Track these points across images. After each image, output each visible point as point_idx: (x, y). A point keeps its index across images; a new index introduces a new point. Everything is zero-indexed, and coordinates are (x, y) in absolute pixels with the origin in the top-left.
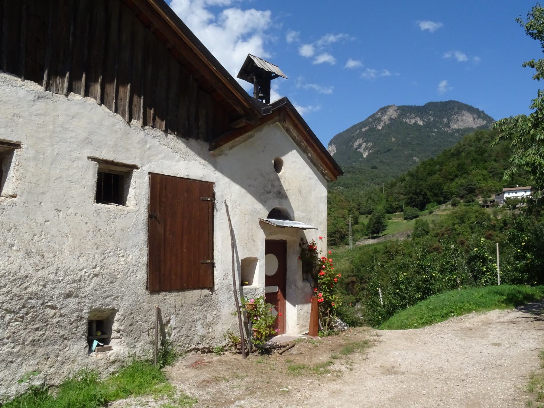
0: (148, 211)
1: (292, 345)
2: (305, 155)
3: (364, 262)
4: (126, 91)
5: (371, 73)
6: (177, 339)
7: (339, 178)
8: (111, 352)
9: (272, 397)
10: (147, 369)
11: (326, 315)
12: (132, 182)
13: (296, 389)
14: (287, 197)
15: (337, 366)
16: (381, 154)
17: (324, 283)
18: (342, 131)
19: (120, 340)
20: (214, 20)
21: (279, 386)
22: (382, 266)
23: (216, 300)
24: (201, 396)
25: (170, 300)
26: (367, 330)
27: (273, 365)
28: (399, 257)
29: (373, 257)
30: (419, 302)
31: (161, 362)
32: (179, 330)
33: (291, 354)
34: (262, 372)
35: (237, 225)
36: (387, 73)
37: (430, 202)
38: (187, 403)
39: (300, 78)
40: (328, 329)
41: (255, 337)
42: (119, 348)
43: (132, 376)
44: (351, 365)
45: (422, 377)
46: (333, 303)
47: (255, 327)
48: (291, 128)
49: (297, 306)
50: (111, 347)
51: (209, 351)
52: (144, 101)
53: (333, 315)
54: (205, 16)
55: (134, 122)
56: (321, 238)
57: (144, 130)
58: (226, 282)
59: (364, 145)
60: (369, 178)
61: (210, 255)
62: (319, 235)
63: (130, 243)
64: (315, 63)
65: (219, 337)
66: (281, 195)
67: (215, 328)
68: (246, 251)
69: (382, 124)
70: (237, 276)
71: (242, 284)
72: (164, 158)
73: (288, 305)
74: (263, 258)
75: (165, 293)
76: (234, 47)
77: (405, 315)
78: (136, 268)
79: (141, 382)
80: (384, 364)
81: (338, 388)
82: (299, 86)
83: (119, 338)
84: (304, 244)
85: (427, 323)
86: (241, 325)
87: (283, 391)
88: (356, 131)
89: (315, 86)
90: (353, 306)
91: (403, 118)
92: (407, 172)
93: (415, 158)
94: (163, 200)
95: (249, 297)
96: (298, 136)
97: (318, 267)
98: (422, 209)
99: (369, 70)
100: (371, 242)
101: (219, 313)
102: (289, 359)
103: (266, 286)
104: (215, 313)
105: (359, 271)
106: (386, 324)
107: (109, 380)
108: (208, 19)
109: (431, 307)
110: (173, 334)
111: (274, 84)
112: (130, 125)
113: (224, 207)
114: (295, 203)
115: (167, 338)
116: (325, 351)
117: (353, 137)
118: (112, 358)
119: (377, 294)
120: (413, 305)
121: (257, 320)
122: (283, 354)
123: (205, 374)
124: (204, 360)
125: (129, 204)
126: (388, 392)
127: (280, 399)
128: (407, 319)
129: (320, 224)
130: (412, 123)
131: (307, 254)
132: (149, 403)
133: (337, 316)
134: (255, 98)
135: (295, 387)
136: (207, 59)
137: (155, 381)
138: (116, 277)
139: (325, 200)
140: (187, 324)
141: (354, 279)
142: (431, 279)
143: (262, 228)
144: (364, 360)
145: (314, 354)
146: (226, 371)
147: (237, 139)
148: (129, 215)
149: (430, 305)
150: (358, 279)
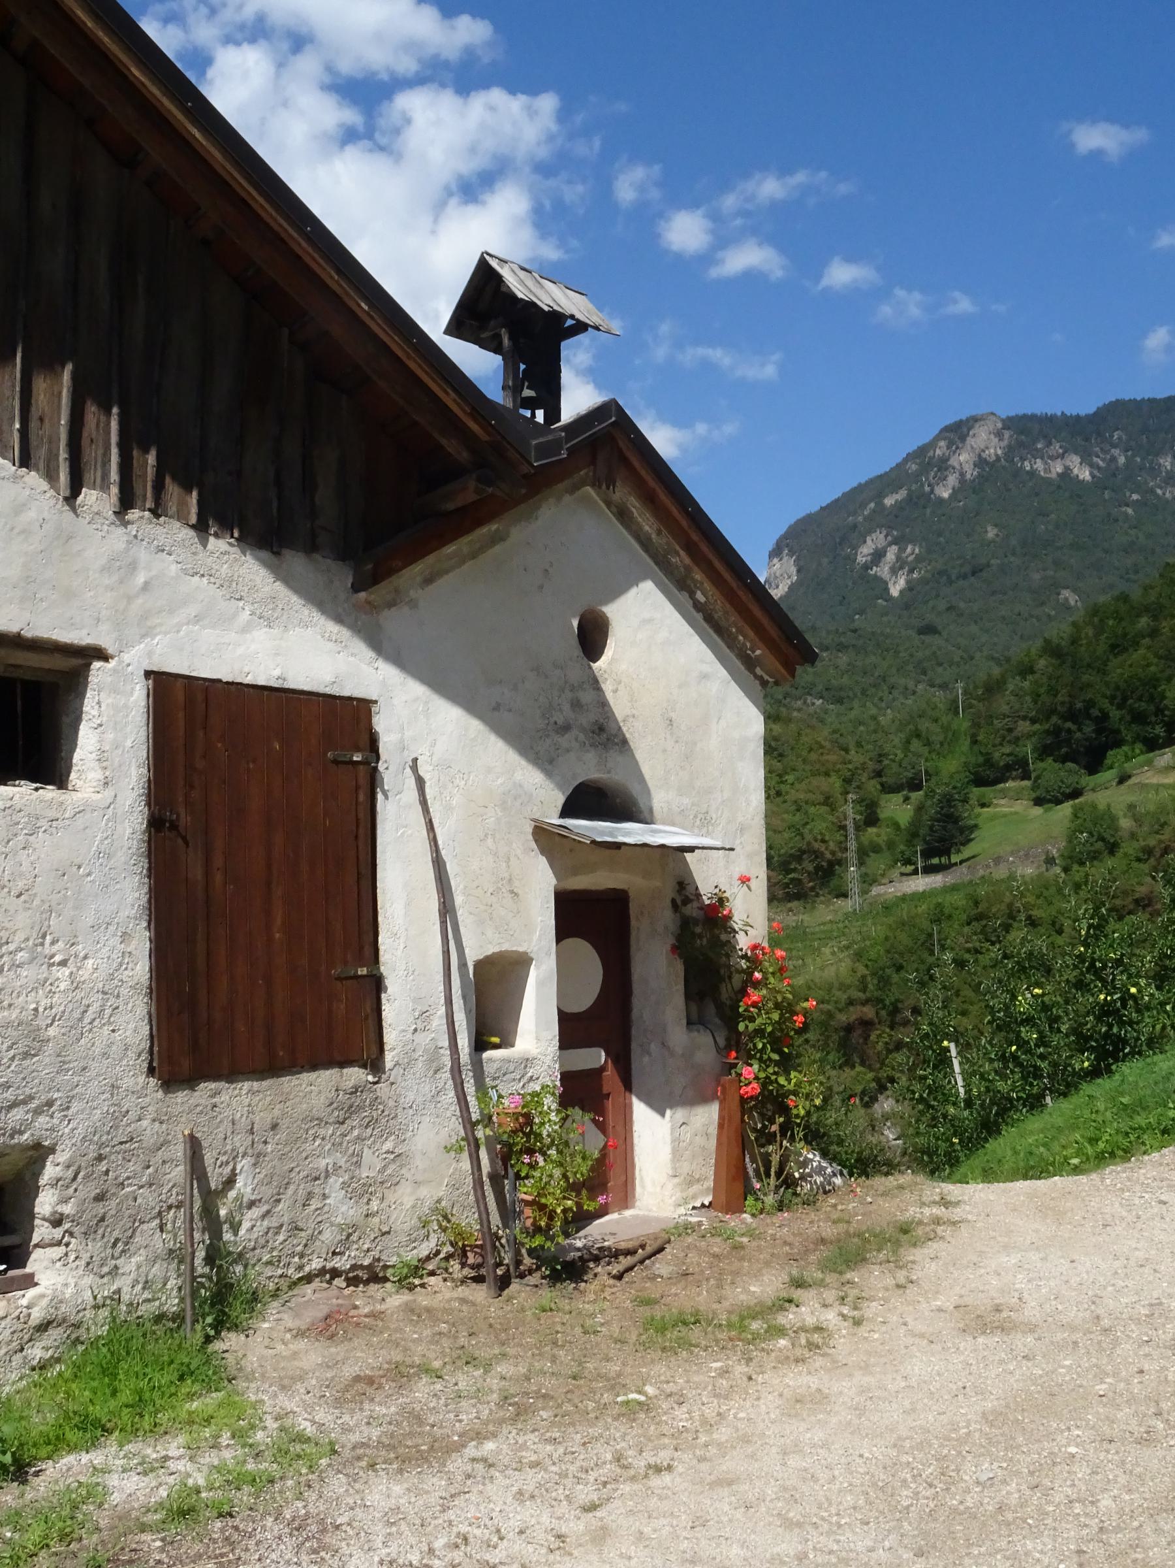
0: (148, 804)
1: (656, 1246)
2: (683, 597)
3: (901, 954)
4: (57, 391)
5: (909, 306)
6: (262, 1241)
7: (805, 674)
8: (31, 1293)
9: (592, 1425)
10: (161, 1348)
11: (771, 1139)
12: (89, 705)
13: (670, 1395)
14: (625, 742)
15: (809, 1311)
16: (950, 582)
17: (759, 1032)
18: (815, 508)
19: (63, 1249)
20: (361, 129)
21: (613, 1387)
22: (960, 964)
23: (391, 1103)
24: (346, 1429)
25: (232, 1107)
26: (912, 1187)
27: (592, 1315)
28: (1017, 935)
29: (930, 935)
30: (1084, 1086)
31: (209, 1320)
32: (265, 1208)
33: (653, 1278)
34: (555, 1343)
35: (457, 842)
36: (964, 305)
37: (1118, 744)
38: (299, 1456)
39: (665, 328)
40: (777, 1188)
41: (529, 1223)
42: (61, 1280)
43: (109, 1371)
44: (856, 1308)
45: (1097, 1337)
46: (791, 1101)
47: (526, 1192)
48: (635, 506)
49: (668, 1112)
50: (32, 1275)
51: (374, 1275)
53: (792, 1140)
54: (332, 114)
55: (89, 497)
56: (745, 880)
57: (126, 524)
58: (423, 1039)
59: (891, 555)
60: (910, 667)
61: (368, 951)
62: (739, 869)
63: (88, 918)
64: (714, 273)
65: (406, 1227)
66: (606, 735)
67: (391, 1197)
68: (489, 933)
69: (952, 480)
70: (460, 1018)
71: (480, 1045)
72: (197, 619)
73: (640, 1111)
74: (548, 954)
75: (213, 1085)
76: (436, 220)
77: (1042, 1131)
79: (140, 1392)
80: (968, 1300)
81: (814, 1387)
82: (661, 353)
83: (59, 1243)
84: (686, 901)
85: (1112, 1154)
86: (478, 1183)
87: (627, 1402)
88: (863, 505)
89: (718, 355)
90: (867, 1105)
91: (1023, 459)
92: (1039, 643)
93: (1066, 593)
94: (200, 764)
95: (504, 1089)
96: (659, 532)
97: (737, 980)
98: (1094, 765)
99: (900, 293)
100: (921, 883)
101: (399, 1147)
102: (645, 1294)
103: (561, 1047)
104: (388, 1145)
105: (884, 982)
106: (979, 1160)
107: (27, 1389)
108: (341, 125)
109: (1125, 1100)
110: (246, 1225)
111: (575, 358)
112: (74, 509)
113: (411, 782)
114: (655, 764)
115: (227, 1236)
116: (767, 1264)
117: (854, 527)
118: (37, 1315)
119: (943, 1061)
120: (1065, 1095)
121: (533, 1166)
122: (626, 1278)
123: (361, 1357)
124: (356, 1307)
125: (79, 783)
126: (981, 1392)
127: (618, 1429)
128: (1045, 1145)
129: (742, 829)
130: (1053, 475)
131: (700, 936)
132: (169, 1463)
133: (808, 1143)
134: (509, 404)
135: (669, 1388)
136: (339, 271)
137: (188, 1386)
138: (44, 1035)
139: (757, 750)
140: (292, 1188)
141: (869, 1012)
142: (1124, 1006)
143: (542, 853)
144: (898, 1286)
145: (732, 1273)
146: (431, 1342)
147: (450, 549)
148: (80, 821)
149: (1122, 1094)
150: (883, 1013)
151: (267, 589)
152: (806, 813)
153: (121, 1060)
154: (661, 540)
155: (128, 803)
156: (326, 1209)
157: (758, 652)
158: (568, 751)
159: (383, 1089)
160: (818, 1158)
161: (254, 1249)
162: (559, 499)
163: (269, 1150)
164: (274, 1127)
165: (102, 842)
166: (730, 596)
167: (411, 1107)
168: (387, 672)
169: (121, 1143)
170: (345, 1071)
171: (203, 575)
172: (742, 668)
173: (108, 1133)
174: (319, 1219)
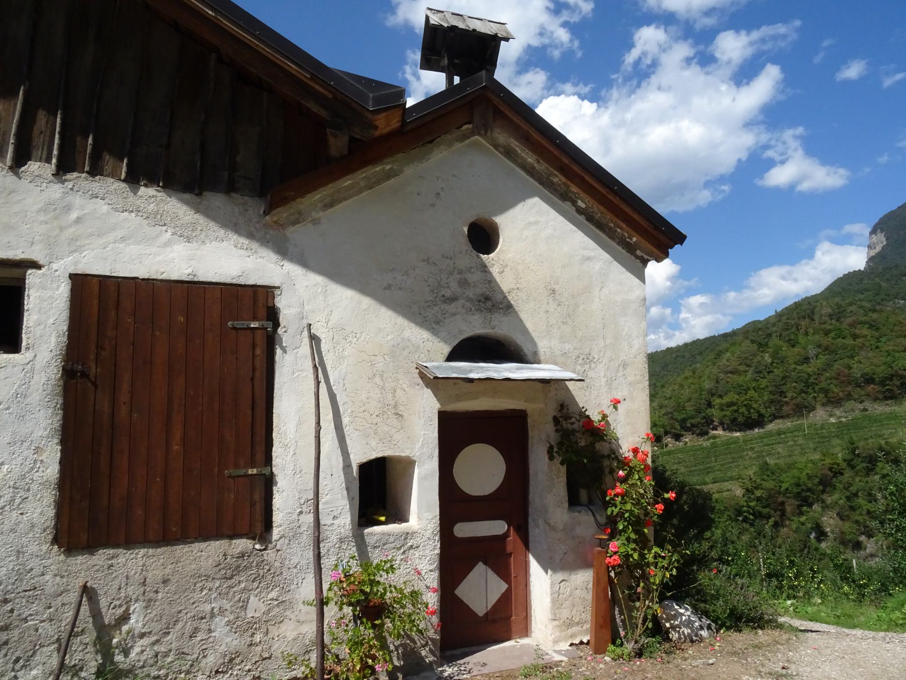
2: (567, 206)
6: (151, 662)
14: (509, 306)
18: (894, 208)
23: (277, 564)
25: (123, 570)
48: (515, 144)
52: (62, 119)
72: (123, 239)
78: (22, 493)
96: (538, 162)
104: (273, 595)
110: (137, 649)
115: (119, 658)
140: (180, 625)
151: (187, 218)
152: (894, 356)
153: (27, 534)
154: (542, 167)
155: (46, 360)
156: (211, 640)
157: (634, 239)
158: (454, 315)
159: (270, 555)
160: (689, 613)
161: (143, 667)
162: (450, 145)
163: (160, 597)
164: (165, 582)
165: (20, 386)
166: (602, 200)
167: (296, 567)
168: (291, 269)
169: (26, 591)
170: (234, 541)
171: (132, 212)
172: (624, 251)
173: (13, 584)
174: (205, 647)
